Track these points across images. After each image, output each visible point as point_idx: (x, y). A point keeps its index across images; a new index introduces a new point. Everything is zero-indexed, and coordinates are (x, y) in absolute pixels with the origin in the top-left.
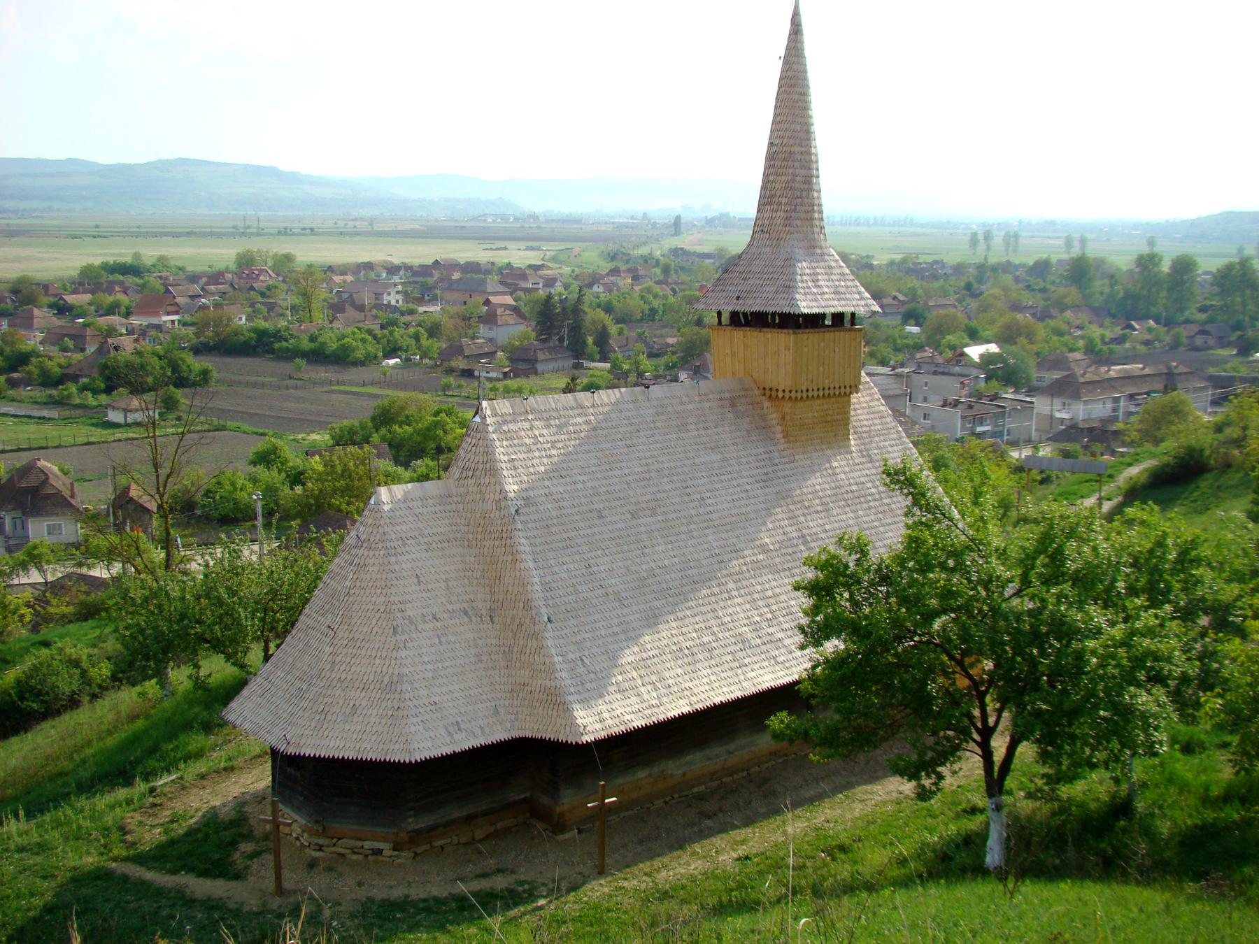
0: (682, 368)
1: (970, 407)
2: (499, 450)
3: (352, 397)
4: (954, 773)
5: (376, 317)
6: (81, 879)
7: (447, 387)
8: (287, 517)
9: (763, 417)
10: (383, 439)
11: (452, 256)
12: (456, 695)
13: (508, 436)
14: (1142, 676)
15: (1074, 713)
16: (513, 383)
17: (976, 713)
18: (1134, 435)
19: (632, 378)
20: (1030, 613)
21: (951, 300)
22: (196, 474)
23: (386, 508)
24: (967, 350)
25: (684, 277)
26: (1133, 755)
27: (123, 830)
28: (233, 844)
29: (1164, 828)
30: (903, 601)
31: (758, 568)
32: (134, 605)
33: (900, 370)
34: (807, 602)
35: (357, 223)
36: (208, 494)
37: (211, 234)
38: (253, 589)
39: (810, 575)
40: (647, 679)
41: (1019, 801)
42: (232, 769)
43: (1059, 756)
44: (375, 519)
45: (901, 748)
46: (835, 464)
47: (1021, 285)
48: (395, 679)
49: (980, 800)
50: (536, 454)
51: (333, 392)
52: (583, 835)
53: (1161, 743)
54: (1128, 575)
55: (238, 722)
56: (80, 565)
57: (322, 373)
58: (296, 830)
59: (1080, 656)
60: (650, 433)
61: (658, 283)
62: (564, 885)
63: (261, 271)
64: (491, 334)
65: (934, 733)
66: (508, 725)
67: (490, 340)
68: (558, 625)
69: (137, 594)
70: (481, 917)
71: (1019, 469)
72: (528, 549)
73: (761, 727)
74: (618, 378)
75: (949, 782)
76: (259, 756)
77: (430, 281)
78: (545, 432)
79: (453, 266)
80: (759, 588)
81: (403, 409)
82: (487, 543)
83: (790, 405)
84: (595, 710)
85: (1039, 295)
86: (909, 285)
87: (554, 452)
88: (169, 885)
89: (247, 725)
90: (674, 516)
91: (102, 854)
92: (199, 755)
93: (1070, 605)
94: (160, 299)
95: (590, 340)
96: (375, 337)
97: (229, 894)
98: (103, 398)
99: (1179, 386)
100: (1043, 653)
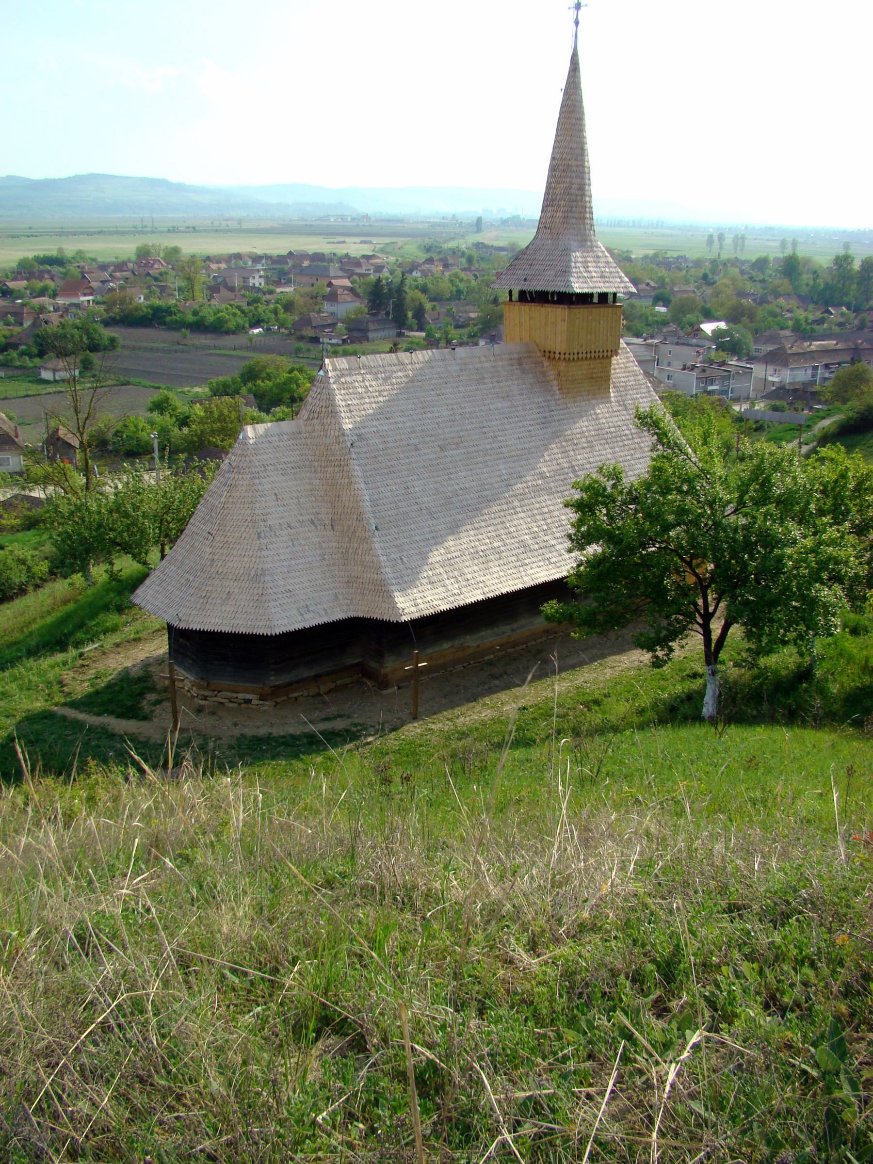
0: (481, 337)
1: (704, 371)
2: (338, 397)
3: (226, 358)
4: (682, 647)
5: (244, 296)
6: (32, 718)
7: (298, 351)
8: (175, 451)
9: (543, 373)
10: (250, 391)
11: (302, 248)
12: (306, 585)
13: (345, 386)
14: (825, 576)
15: (773, 603)
16: (349, 348)
17: (700, 602)
18: (828, 396)
19: (443, 343)
20: (745, 528)
21: (692, 287)
22: (106, 419)
23: (251, 441)
24: (703, 326)
25: (484, 265)
26: (814, 635)
27: (61, 683)
28: (141, 694)
29: (834, 689)
30: (648, 516)
31: (538, 490)
32: (63, 517)
33: (650, 341)
34: (573, 516)
35: (229, 223)
36: (117, 434)
37: (117, 233)
38: (150, 506)
39: (577, 496)
40: (451, 574)
41: (730, 668)
42: (139, 639)
43: (761, 635)
44: (243, 450)
45: (644, 627)
46: (598, 411)
47: (746, 277)
48: (259, 572)
49: (700, 667)
50: (367, 400)
51: (211, 355)
52: (401, 691)
53: (836, 627)
54: (818, 500)
55: (142, 605)
56: (24, 488)
57: (203, 340)
58: (187, 685)
59: (780, 559)
60: (454, 385)
61: (464, 270)
62: (387, 727)
63: (155, 261)
64: (333, 309)
65: (668, 617)
66: (345, 608)
67: (333, 314)
68: (383, 532)
69: (65, 509)
70: (326, 749)
71: (739, 419)
72: (360, 474)
73: (535, 611)
74: (431, 343)
75: (677, 654)
76: (159, 630)
77: (286, 268)
78: (374, 383)
79: (304, 256)
80: (537, 506)
81: (265, 367)
82: (329, 469)
83: (564, 364)
84: (411, 597)
85: (759, 285)
86: (659, 275)
87: (381, 399)
88: (97, 724)
89: (149, 607)
90: (473, 449)
91: (47, 701)
92: (114, 629)
93: (774, 521)
94: (78, 283)
95: (410, 314)
96: (243, 312)
97: (140, 730)
98: (37, 360)
99: (863, 358)
100: (752, 557)
